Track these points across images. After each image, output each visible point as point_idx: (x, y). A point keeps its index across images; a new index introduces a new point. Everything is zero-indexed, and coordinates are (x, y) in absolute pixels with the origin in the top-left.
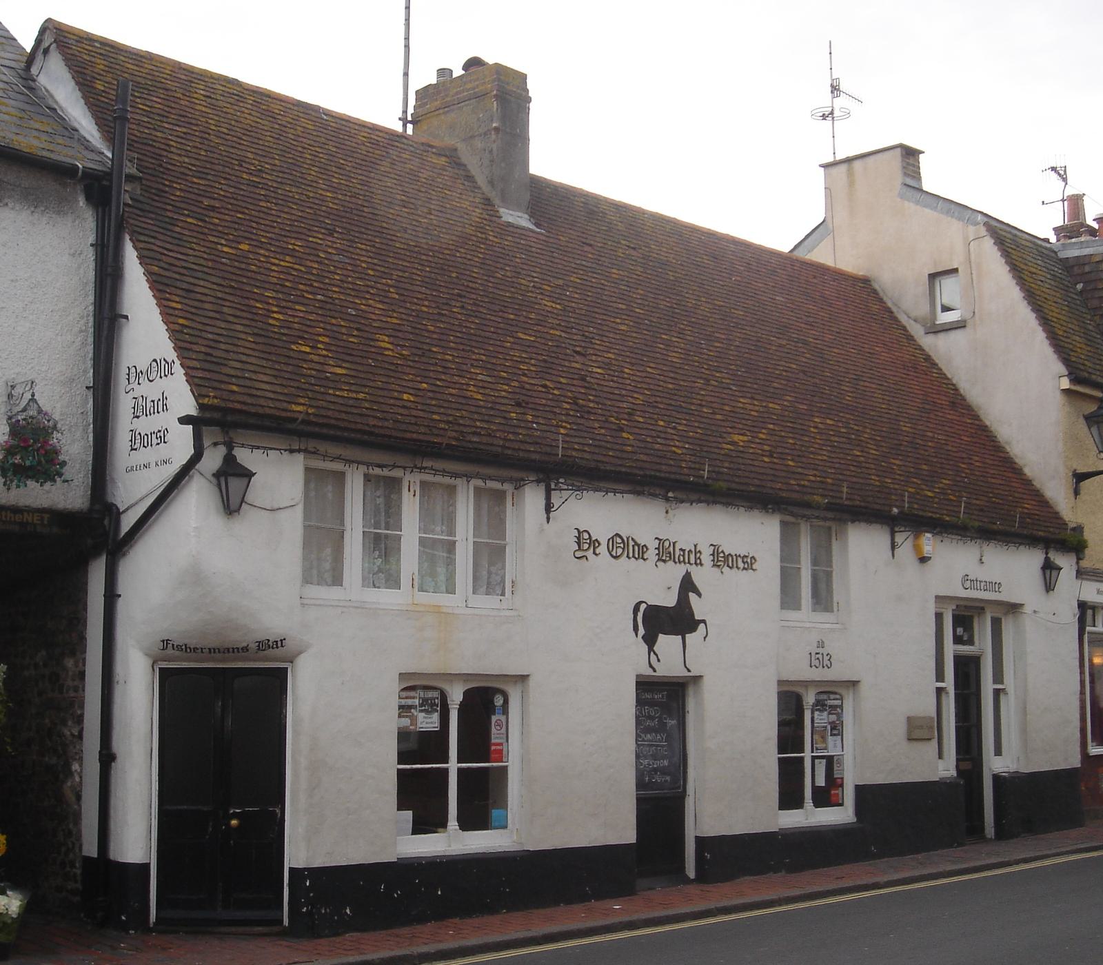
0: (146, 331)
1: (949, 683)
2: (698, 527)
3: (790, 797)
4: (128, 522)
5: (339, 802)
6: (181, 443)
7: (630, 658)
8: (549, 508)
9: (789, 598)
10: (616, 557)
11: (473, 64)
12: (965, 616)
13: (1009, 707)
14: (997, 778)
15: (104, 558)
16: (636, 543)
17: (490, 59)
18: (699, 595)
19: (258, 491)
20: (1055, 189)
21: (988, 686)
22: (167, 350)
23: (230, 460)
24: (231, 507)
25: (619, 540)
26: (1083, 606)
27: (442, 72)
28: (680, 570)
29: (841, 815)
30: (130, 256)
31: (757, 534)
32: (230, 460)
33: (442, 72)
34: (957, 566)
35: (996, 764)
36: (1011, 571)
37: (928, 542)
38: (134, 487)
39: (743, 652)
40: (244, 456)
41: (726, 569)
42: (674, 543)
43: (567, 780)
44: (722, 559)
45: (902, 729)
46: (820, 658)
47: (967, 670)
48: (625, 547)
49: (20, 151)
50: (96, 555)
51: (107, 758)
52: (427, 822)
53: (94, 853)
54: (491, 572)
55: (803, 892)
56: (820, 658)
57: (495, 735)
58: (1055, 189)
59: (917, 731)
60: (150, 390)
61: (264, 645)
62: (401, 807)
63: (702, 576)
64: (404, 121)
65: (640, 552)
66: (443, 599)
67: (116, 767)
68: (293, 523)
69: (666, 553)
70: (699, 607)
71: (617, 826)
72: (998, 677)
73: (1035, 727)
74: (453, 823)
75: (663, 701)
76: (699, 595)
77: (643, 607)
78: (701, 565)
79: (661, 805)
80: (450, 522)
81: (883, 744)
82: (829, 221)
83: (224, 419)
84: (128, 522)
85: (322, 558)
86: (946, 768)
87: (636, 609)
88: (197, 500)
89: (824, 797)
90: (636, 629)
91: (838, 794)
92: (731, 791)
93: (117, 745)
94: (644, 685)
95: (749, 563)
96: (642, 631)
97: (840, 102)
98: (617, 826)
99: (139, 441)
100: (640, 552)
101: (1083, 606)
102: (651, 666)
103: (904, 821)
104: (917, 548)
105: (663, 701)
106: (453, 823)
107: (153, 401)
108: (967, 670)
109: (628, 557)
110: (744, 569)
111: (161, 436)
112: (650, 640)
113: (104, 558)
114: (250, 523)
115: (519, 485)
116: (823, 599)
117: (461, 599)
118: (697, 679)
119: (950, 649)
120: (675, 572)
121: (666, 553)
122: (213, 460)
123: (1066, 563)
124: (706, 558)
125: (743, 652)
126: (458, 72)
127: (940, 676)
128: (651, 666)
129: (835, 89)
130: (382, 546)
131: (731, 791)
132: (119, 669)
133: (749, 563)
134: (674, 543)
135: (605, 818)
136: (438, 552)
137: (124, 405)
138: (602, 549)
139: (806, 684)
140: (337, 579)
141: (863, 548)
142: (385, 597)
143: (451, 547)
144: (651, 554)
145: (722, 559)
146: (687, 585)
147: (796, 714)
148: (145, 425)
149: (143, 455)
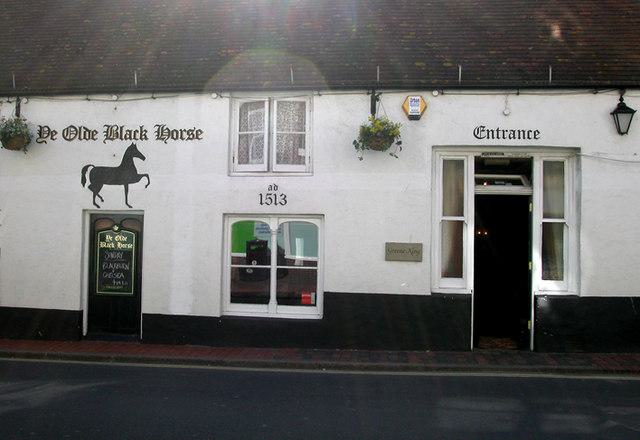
10: (70, 140)
16: (87, 130)
18: (143, 158)
25: (73, 129)
28: (128, 143)
29: (312, 313)
41: (170, 140)
42: (121, 128)
44: (164, 134)
45: (382, 251)
49: (562, 263)
55: (241, 291)
65: (91, 135)
69: (113, 133)
73: (584, 267)
76: (143, 158)
77: (90, 168)
78: (146, 138)
87: (85, 170)
90: (84, 181)
91: (310, 298)
96: (88, 183)
100: (91, 135)
102: (95, 204)
107: (130, 132)
109: (80, 138)
110: (189, 138)
112: (95, 188)
120: (120, 147)
121: (113, 133)
124: (151, 134)
128: (95, 204)
134: (121, 128)
138: (59, 136)
144: (101, 136)
145: (164, 134)
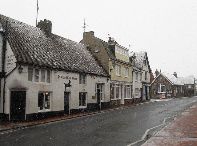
0: (9, 51)
1: (97, 92)
2: (71, 75)
3: (80, 105)
4: (7, 74)
5: (32, 106)
6: (15, 65)
7: (63, 90)
8: (55, 73)
9: (80, 83)
11: (45, 20)
12: (99, 85)
13: (103, 95)
14: (101, 103)
15: (3, 78)
17: (47, 20)
19: (23, 71)
20: (108, 36)
21: (101, 92)
22: (12, 54)
23: (20, 67)
24: (20, 73)
26: (111, 84)
27: (41, 20)
28: (69, 80)
30: (7, 42)
31: (77, 76)
32: (20, 67)
33: (41, 20)
34: (98, 80)
35: (102, 101)
36: (104, 80)
37: (95, 77)
38: (8, 70)
39: (76, 88)
40: (22, 67)
43: (56, 103)
44: (73, 79)
46: (84, 89)
47: (99, 90)
48: (63, 77)
50: (2, 77)
51: (4, 101)
52: (80, 105)
53: (2, 113)
54: (49, 80)
56: (84, 89)
57: (49, 98)
58: (108, 36)
59: (94, 97)
60: (10, 59)
61: (23, 88)
62: (39, 106)
63: (71, 80)
64: (36, 26)
66: (43, 83)
67: (5, 102)
68: (27, 74)
69: (67, 78)
70: (71, 84)
71: (62, 108)
72: (102, 92)
74: (44, 108)
75: (67, 94)
79: (66, 105)
80: (32, 72)
81: (90, 99)
82: (112, 57)
83: (20, 63)
84: (7, 74)
85: (30, 79)
86: (96, 102)
88: (16, 72)
89: (84, 105)
92: (74, 104)
93: (5, 100)
94: (65, 93)
95: (76, 79)
97: (85, 26)
98: (62, 108)
99: (8, 64)
101: (111, 84)
103: (93, 108)
104: (94, 77)
105: (67, 94)
106: (44, 108)
108: (99, 90)
111: (12, 64)
112: (66, 88)
113: (3, 78)
114: (22, 74)
115: (52, 70)
116: (84, 83)
117: (45, 83)
118: (70, 92)
119: (97, 88)
122: (18, 67)
123: (109, 79)
124: (72, 79)
125: (76, 88)
126: (43, 21)
127: (96, 91)
129: (85, 24)
130: (37, 77)
131: (74, 104)
132: (6, 91)
133: (76, 79)
135: (60, 108)
136: (43, 78)
137: (6, 60)
138: (61, 77)
139: (82, 92)
140: (32, 81)
141: (88, 78)
142: (37, 83)
143: (38, 76)
144: (66, 78)
145: (73, 79)
146: (70, 82)
147: (82, 96)
148: (9, 62)
149: (9, 66)
